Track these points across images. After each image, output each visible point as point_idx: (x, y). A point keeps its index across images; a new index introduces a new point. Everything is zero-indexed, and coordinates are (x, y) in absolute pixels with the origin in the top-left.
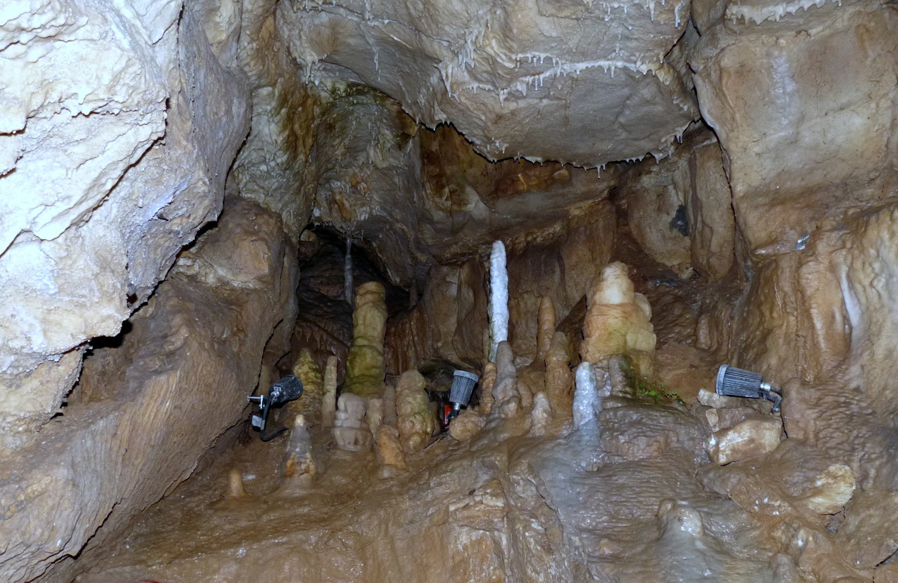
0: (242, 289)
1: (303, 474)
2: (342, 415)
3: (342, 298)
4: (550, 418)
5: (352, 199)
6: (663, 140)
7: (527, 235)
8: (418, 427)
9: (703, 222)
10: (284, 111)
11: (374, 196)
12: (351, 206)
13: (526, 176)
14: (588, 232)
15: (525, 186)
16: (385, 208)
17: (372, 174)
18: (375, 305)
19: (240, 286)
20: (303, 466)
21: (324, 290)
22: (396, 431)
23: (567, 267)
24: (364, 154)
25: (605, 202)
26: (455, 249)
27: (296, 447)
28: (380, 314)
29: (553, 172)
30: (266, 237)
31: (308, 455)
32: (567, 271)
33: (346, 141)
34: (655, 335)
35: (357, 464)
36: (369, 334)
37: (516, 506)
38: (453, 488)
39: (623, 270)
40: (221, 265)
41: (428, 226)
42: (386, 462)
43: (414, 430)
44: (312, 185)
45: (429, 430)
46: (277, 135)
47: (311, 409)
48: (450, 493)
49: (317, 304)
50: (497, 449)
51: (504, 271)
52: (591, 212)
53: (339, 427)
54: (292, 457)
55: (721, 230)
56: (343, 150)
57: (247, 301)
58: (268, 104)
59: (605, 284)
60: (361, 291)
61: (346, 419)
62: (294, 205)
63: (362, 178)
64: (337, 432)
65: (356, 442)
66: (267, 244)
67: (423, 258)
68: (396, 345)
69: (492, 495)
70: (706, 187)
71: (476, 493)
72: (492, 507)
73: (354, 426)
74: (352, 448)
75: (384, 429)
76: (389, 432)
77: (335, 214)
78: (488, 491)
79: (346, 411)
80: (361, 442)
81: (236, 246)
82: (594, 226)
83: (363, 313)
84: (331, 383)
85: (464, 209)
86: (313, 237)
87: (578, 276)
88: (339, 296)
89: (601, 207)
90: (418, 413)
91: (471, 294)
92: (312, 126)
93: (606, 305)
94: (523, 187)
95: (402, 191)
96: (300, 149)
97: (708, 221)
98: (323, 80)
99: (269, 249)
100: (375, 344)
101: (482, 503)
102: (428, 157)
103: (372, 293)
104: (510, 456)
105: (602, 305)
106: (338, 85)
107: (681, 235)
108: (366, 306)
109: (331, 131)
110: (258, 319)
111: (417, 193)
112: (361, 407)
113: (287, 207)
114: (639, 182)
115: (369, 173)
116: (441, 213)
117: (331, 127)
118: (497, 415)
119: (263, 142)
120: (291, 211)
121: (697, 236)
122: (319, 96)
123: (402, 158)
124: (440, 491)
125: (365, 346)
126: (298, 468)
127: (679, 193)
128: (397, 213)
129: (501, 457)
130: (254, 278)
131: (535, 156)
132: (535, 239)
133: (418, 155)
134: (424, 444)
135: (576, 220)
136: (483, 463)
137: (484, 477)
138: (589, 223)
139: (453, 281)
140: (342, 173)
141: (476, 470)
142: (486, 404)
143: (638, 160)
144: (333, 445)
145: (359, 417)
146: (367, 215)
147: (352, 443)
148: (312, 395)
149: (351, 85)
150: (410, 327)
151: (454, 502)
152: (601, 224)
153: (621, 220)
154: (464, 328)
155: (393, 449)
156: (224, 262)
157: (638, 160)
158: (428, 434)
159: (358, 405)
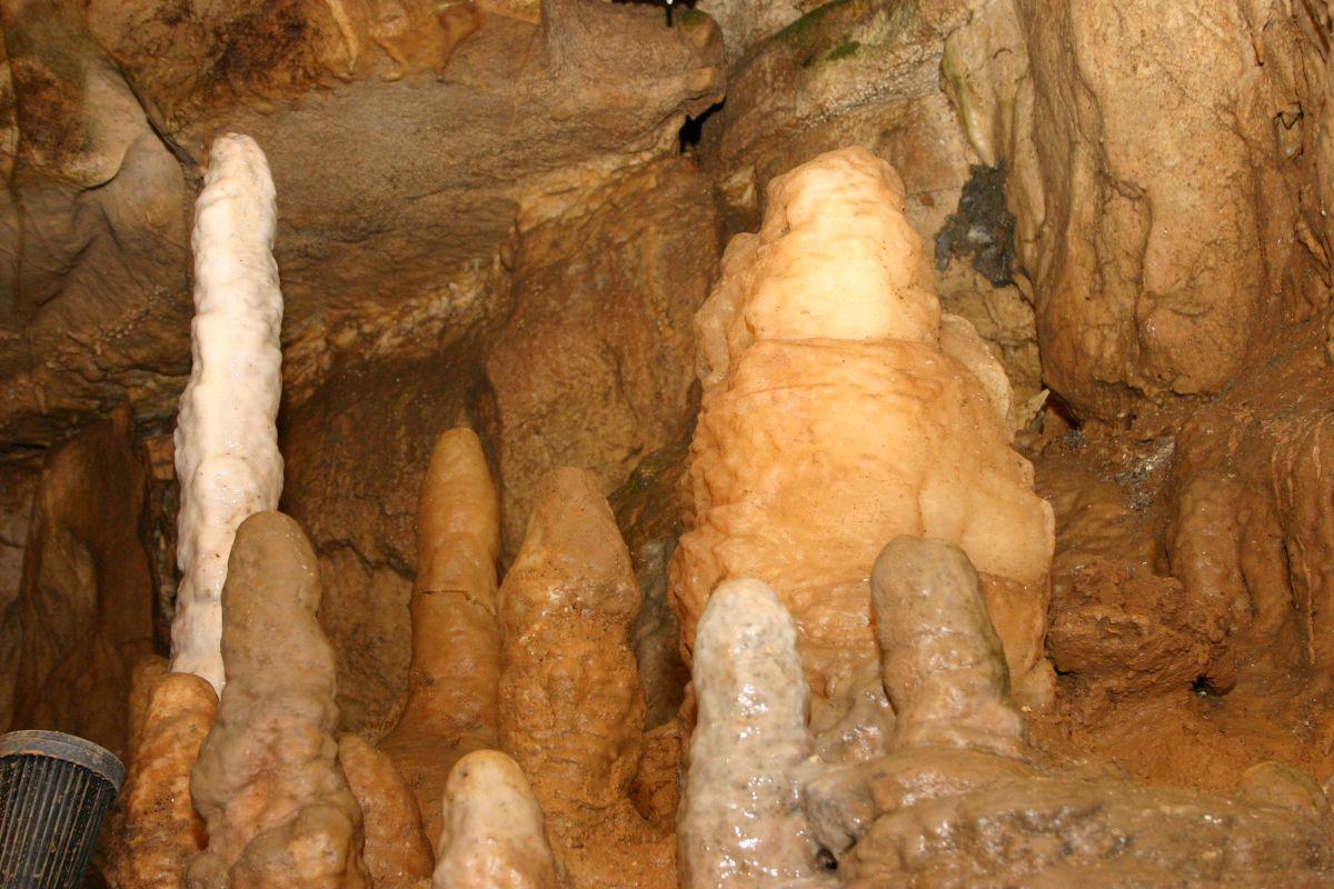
7: (336, 327)
9: (1104, 176)
14: (600, 280)
15: (354, 45)
23: (511, 421)
25: (667, 163)
32: (510, 438)
39: (884, 183)
52: (621, 204)
55: (1186, 199)
59: (797, 246)
70: (1122, 30)
82: (630, 254)
85: (77, 167)
89: (653, 183)
91: (84, 574)
94: (343, 48)
97: (1127, 167)
105: (790, 343)
107: (984, 285)
114: (802, 86)
121: (1075, 248)
127: (974, 118)
132: (371, 339)
135: (549, 236)
138: (606, 242)
152: (656, 244)
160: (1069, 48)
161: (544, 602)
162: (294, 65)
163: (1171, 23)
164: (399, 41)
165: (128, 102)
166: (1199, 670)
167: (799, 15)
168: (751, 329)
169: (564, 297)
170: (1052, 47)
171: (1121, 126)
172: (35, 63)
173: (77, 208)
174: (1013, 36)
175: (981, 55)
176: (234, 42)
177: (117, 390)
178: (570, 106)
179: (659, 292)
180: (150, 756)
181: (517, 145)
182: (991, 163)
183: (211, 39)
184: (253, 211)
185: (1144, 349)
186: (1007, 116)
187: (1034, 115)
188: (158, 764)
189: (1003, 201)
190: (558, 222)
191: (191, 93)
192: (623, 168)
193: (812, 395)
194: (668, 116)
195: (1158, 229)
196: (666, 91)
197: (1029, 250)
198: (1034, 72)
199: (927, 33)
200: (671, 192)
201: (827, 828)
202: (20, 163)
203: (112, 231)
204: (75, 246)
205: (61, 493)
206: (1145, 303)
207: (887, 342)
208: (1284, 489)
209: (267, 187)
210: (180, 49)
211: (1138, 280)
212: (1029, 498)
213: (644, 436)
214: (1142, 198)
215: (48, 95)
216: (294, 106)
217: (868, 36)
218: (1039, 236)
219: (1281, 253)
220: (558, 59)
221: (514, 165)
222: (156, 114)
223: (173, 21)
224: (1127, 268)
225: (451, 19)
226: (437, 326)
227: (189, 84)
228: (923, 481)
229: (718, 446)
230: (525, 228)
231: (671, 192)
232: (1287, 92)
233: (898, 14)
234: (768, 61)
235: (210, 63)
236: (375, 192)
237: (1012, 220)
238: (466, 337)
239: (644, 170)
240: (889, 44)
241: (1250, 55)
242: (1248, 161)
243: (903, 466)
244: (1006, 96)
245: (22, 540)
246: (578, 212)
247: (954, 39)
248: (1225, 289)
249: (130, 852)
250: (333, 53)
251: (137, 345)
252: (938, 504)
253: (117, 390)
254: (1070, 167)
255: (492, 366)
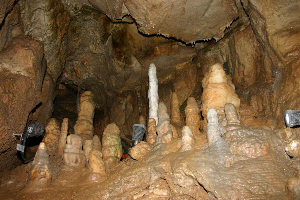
0: (16, 75)
1: (42, 178)
2: (69, 146)
3: (75, 112)
4: (194, 141)
5: (81, 69)
6: (221, 29)
8: (112, 153)
9: (239, 63)
10: (52, 10)
11: (91, 68)
12: (81, 72)
13: (160, 48)
16: (95, 74)
17: (90, 57)
18: (90, 101)
19: (16, 73)
20: (42, 173)
21: (67, 109)
22: (101, 153)
24: (88, 48)
26: (125, 89)
27: (38, 162)
28: (91, 105)
29: (172, 46)
30: (33, 49)
31: (46, 167)
33: (80, 40)
34: (239, 99)
35: (76, 173)
36: (86, 114)
37: (179, 193)
38: (136, 185)
40: (6, 62)
41: (114, 76)
42: (95, 171)
43: (110, 155)
44: (64, 56)
45: (119, 156)
46: (48, 21)
47: (53, 148)
48: (135, 188)
49: (64, 113)
50: (164, 159)
51: (156, 77)
53: (67, 152)
54: (35, 167)
55: (248, 66)
56: (78, 44)
57: (18, 80)
58: (44, 3)
59: (213, 73)
60: (83, 95)
61: (71, 148)
62: (55, 62)
63: (86, 59)
64: (66, 156)
65: (76, 161)
66: (33, 52)
67: (110, 95)
68: (98, 132)
69: (160, 188)
71: (150, 188)
72: (160, 196)
73: (75, 152)
74: (73, 164)
75: (93, 152)
76: (96, 153)
77: (74, 77)
78: (158, 186)
79: (71, 144)
80: (79, 160)
81: (15, 52)
82: (188, 72)
83: (84, 105)
84: (64, 132)
85: (130, 66)
86: (64, 88)
87: (181, 94)
88: (74, 111)
90: (114, 146)
91: (132, 107)
92: (65, 25)
93: (215, 83)
95: (103, 65)
96: (59, 33)
97: (242, 62)
98: (71, 3)
99: (34, 55)
100: (89, 119)
101: (154, 194)
102: (115, 44)
103: (88, 96)
104: (172, 163)
106: (78, 6)
108: (85, 102)
109: (74, 33)
110: (24, 91)
111: (110, 64)
112: (80, 142)
113: (51, 63)
115: (89, 57)
116: (120, 68)
117: (74, 31)
118: (159, 142)
119: (41, 24)
120: (54, 65)
121: (236, 71)
122: (70, 12)
123: (103, 49)
124: (128, 186)
125: (83, 120)
126: (39, 175)
128: (100, 76)
129: (166, 164)
130: (24, 69)
131: (166, 33)
133: (111, 46)
134: (114, 162)
135: (179, 71)
136: (154, 168)
137: (155, 177)
138: (185, 71)
139: (123, 103)
140: (78, 57)
141: (150, 173)
142: (151, 139)
143: (209, 40)
144: (63, 162)
145: (79, 147)
146: (87, 77)
147: (74, 162)
148: (55, 141)
149: (84, 7)
150: (104, 123)
151: (137, 194)
152: (190, 71)
153: (198, 70)
154: (128, 122)
155: (98, 163)
156: (8, 60)
157: (209, 40)
158: (118, 158)
159: (78, 141)
160: (235, 50)
161: (190, 110)
162: (153, 55)
163: (246, 47)
164: (164, 52)
165: (136, 59)
166: (255, 115)
167: (204, 47)
168: (209, 82)
169: (181, 77)
170: (233, 50)
171: (241, 58)
172: (126, 56)
173: (130, 70)
174: (228, 49)
175: (225, 50)
176: (147, 53)
177: (134, 88)
178: (181, 57)
179: (191, 76)
180: (149, 126)
181: (176, 62)
182: (226, 62)
183: (144, 52)
184: (154, 71)
185: (244, 81)
186: (228, 57)
187: (231, 57)
188: (150, 127)
189: (228, 66)
190: (180, 69)
191: (143, 58)
192: (187, 63)
193: (215, 89)
194: (191, 58)
195: (245, 69)
196: (191, 55)
197: (231, 71)
198: (230, 52)
199: (219, 48)
200: (192, 66)
201: (222, 133)
202: (125, 66)
203: (134, 72)
204: (130, 74)
205: (129, 99)
206: (244, 76)
207: (223, 83)
208: (262, 96)
209: (155, 68)
210: (141, 54)
211: (243, 74)
212: (237, 98)
213: (190, 91)
214: (244, 66)
215: (128, 59)
216: (153, 59)
217: (212, 49)
218: (232, 69)
219: (259, 71)
220: (180, 53)
221: (175, 63)
222: (139, 60)
223: (140, 51)
224: (242, 73)
225: (169, 49)
226: (167, 80)
227: (142, 57)
228: (227, 97)
229: (206, 94)
230: (176, 70)
231: (192, 66)
232: (259, 54)
233: (215, 47)
234: (201, 52)
235: (144, 55)
236: (161, 67)
237: (229, 68)
238: (170, 82)
239: (189, 64)
240: (214, 50)
241: (255, 50)
242: (255, 61)
243: (225, 96)
244: (228, 55)
245: (125, 104)
246: (182, 68)
247: (222, 49)
248: (253, 75)
249: (148, 136)
250: (157, 53)
251: (136, 83)
252: (229, 100)
253: (134, 88)
254: (235, 62)
255: (174, 85)
